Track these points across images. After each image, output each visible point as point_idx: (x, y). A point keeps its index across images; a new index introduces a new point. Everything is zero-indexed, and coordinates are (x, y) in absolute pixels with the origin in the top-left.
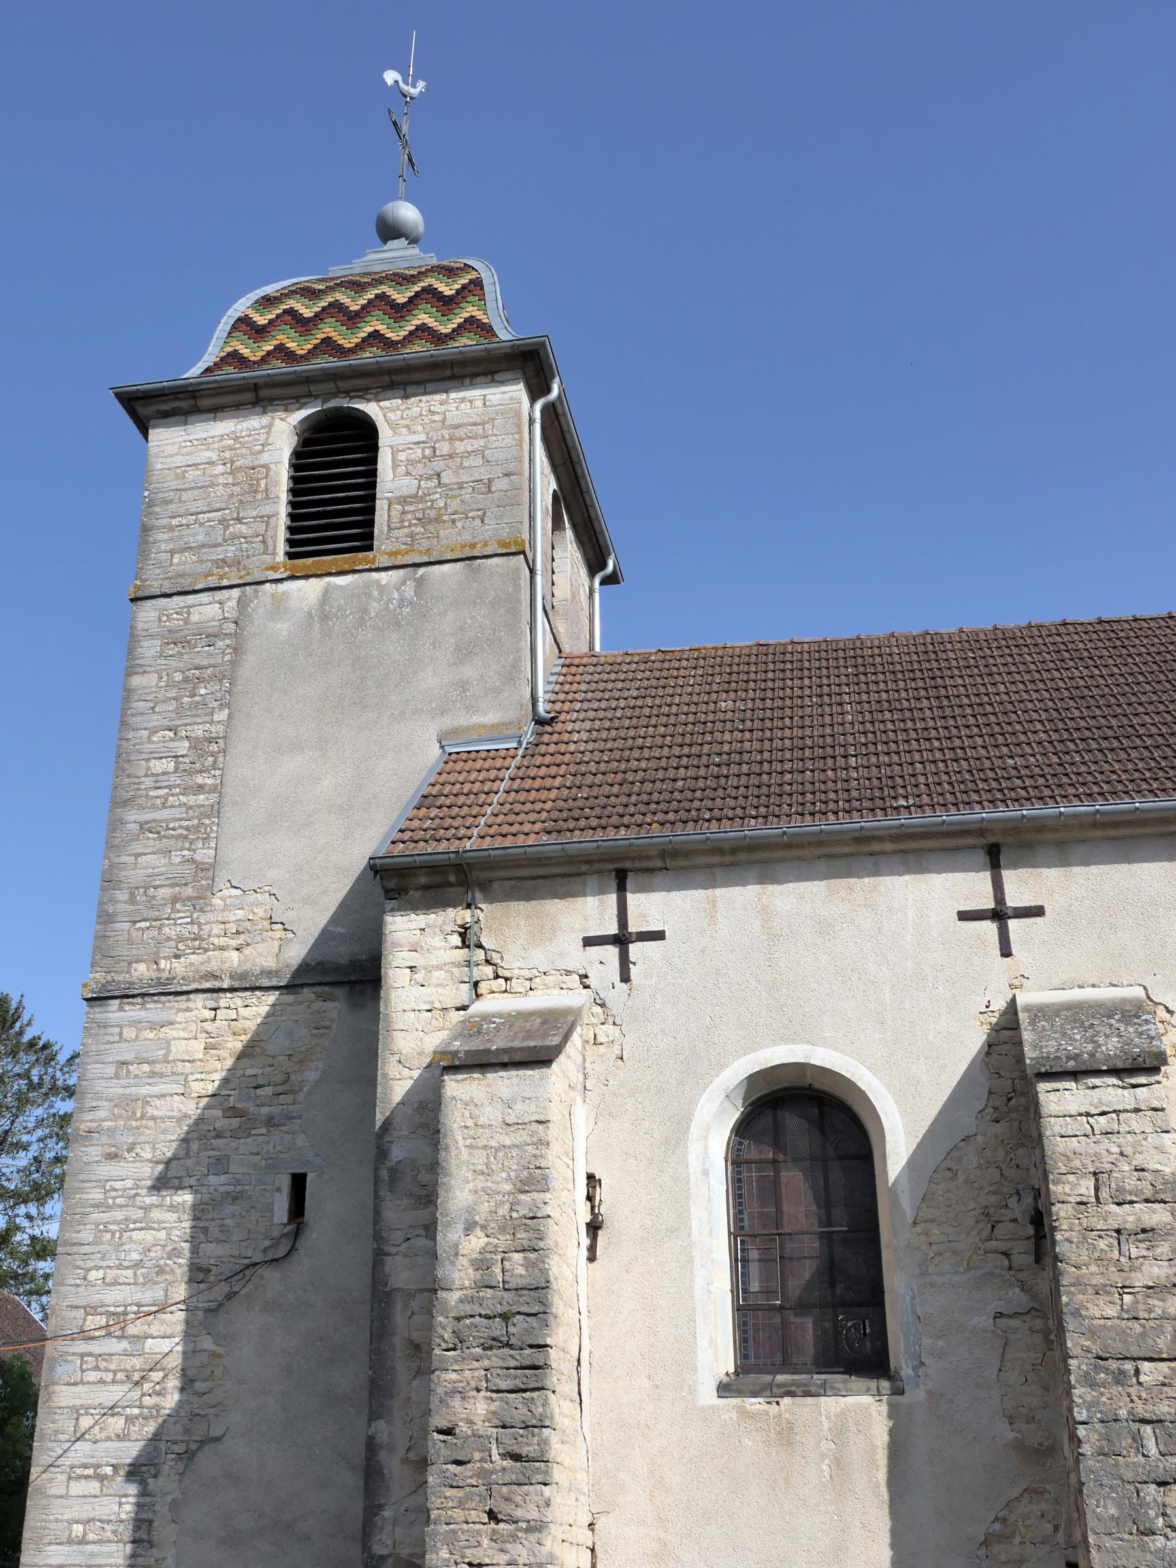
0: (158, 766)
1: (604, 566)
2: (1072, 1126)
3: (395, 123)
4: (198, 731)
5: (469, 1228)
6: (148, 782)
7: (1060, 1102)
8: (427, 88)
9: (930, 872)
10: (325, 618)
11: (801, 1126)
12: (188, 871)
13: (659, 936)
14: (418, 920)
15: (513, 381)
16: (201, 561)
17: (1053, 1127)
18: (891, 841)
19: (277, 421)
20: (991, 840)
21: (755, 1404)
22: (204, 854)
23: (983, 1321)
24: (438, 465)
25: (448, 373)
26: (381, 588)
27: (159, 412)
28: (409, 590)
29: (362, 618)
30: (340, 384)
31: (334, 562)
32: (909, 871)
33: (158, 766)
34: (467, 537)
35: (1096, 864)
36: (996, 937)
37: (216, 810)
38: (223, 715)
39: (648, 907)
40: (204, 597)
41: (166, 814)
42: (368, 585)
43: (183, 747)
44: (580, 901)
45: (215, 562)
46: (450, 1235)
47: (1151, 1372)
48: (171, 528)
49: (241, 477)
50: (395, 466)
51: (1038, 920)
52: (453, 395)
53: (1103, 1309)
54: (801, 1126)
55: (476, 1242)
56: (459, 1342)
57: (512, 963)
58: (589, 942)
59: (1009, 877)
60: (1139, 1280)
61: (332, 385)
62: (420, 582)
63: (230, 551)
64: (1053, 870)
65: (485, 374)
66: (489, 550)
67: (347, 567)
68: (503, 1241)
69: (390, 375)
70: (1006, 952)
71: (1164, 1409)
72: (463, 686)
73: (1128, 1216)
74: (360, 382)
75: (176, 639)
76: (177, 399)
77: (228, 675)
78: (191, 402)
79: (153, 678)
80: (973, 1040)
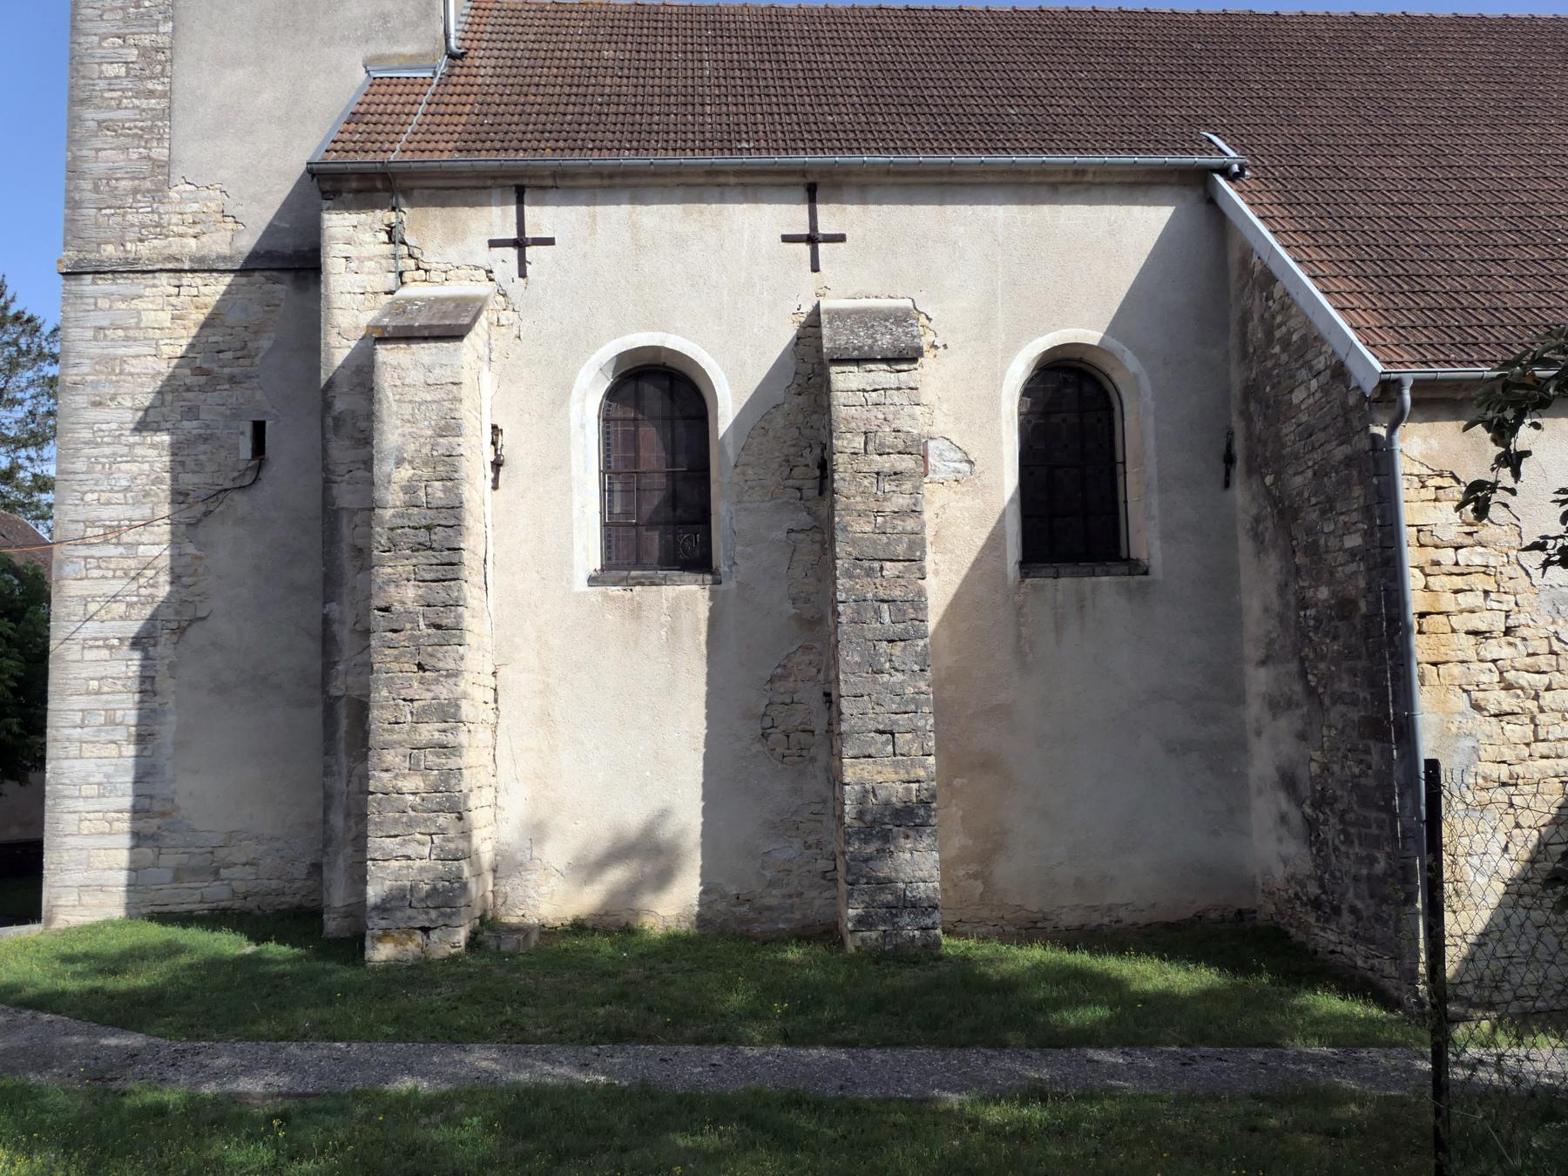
2: (852, 399)
4: (146, 41)
5: (399, 462)
6: (102, 84)
7: (845, 380)
11: (656, 393)
12: (146, 167)
13: (549, 242)
17: (839, 398)
20: (811, 179)
21: (615, 591)
22: (160, 153)
23: (780, 534)
32: (747, 201)
37: (167, 114)
38: (167, 27)
39: (542, 218)
41: (121, 114)
46: (384, 468)
53: (862, 527)
54: (656, 393)
55: (405, 473)
57: (430, 258)
58: (493, 244)
60: (889, 507)
68: (426, 472)
70: (815, 268)
71: (897, 593)
73: (885, 463)
80: (788, 333)
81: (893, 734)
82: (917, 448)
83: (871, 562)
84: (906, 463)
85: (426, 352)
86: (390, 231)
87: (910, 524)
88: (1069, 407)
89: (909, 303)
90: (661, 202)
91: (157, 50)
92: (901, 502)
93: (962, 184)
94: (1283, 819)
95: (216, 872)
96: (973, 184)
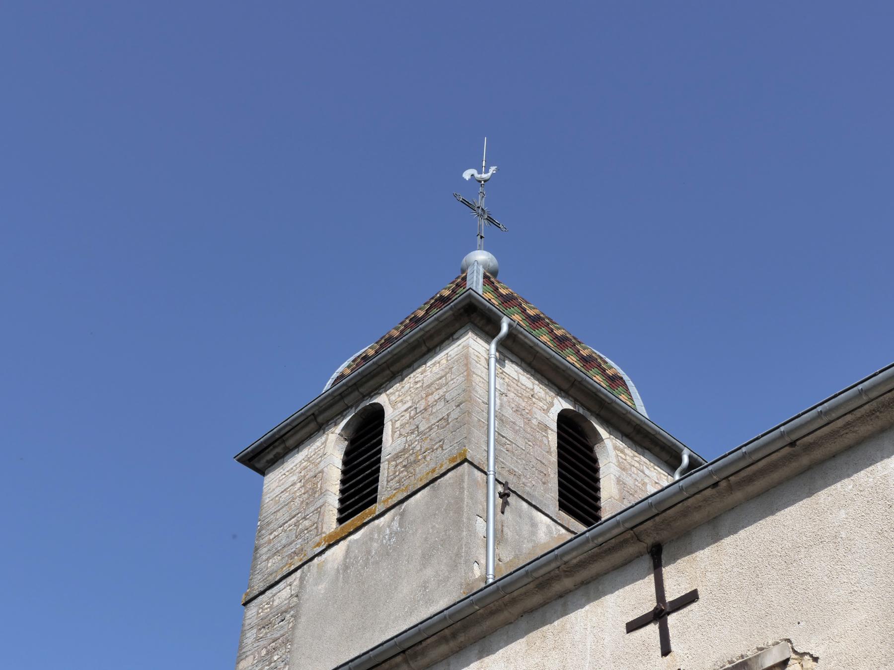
1: (680, 460)
3: (464, 202)
8: (498, 170)
9: (605, 594)
15: (466, 333)
18: (567, 576)
19: (330, 435)
20: (650, 541)
25: (424, 349)
26: (380, 529)
27: (268, 462)
29: (368, 559)
30: (361, 390)
31: (352, 524)
32: (589, 600)
35: (743, 527)
36: (658, 638)
42: (371, 532)
51: (693, 606)
52: (429, 364)
61: (356, 393)
64: (706, 550)
65: (447, 338)
67: (359, 523)
69: (389, 368)
74: (372, 383)
76: (275, 447)
78: (282, 446)
81: (466, 460)
90: (507, 643)
93: (834, 456)
94: (390, 340)
96: (849, 448)
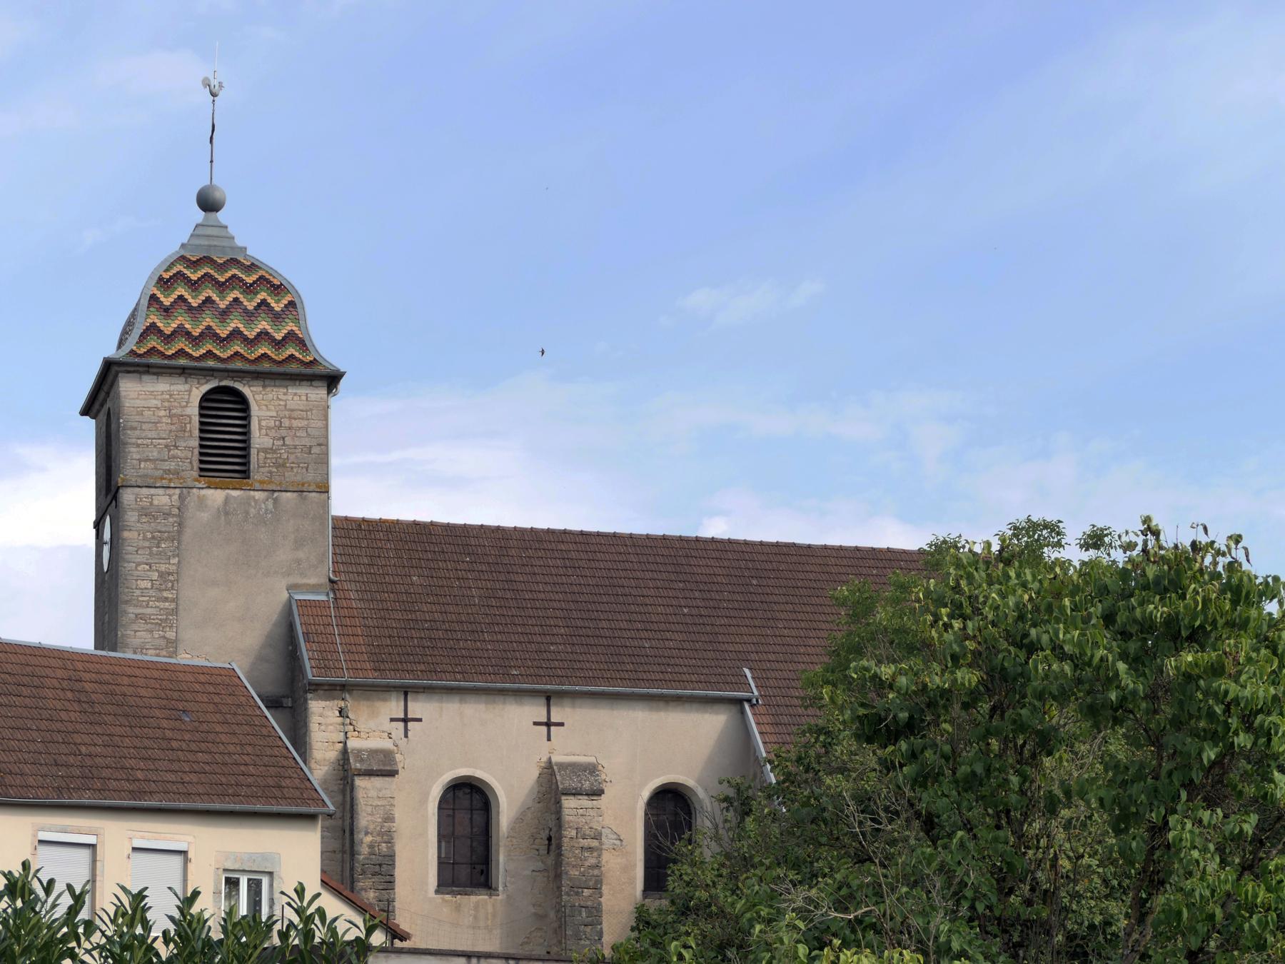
0: (144, 584)
2: (571, 812)
4: (163, 568)
5: (367, 833)
6: (138, 592)
7: (569, 803)
10: (227, 514)
11: (467, 801)
12: (163, 643)
13: (420, 720)
14: (323, 703)
16: (156, 469)
17: (566, 812)
21: (448, 897)
22: (171, 635)
23: (528, 872)
24: (283, 432)
26: (256, 501)
28: (270, 504)
33: (144, 584)
34: (299, 478)
37: (175, 611)
38: (175, 561)
39: (418, 707)
40: (161, 491)
41: (149, 611)
43: (155, 576)
44: (388, 704)
45: (165, 471)
46: (359, 836)
47: (586, 892)
48: (138, 446)
49: (175, 420)
50: (260, 429)
53: (574, 873)
54: (467, 801)
55: (369, 839)
56: (364, 872)
57: (361, 726)
58: (392, 720)
59: (553, 710)
60: (587, 864)
62: (276, 500)
63: (172, 465)
66: (311, 489)
68: (379, 839)
70: (549, 739)
71: (589, 903)
72: (299, 562)
73: (585, 843)
75: (144, 512)
77: (177, 537)
79: (136, 534)
80: (534, 773)
82: (598, 836)
83: (576, 889)
84: (595, 843)
85: (378, 782)
86: (342, 712)
87: (596, 872)
88: (670, 806)
89: (592, 760)
91: (169, 574)
92: (592, 861)
95: (688, 908)
